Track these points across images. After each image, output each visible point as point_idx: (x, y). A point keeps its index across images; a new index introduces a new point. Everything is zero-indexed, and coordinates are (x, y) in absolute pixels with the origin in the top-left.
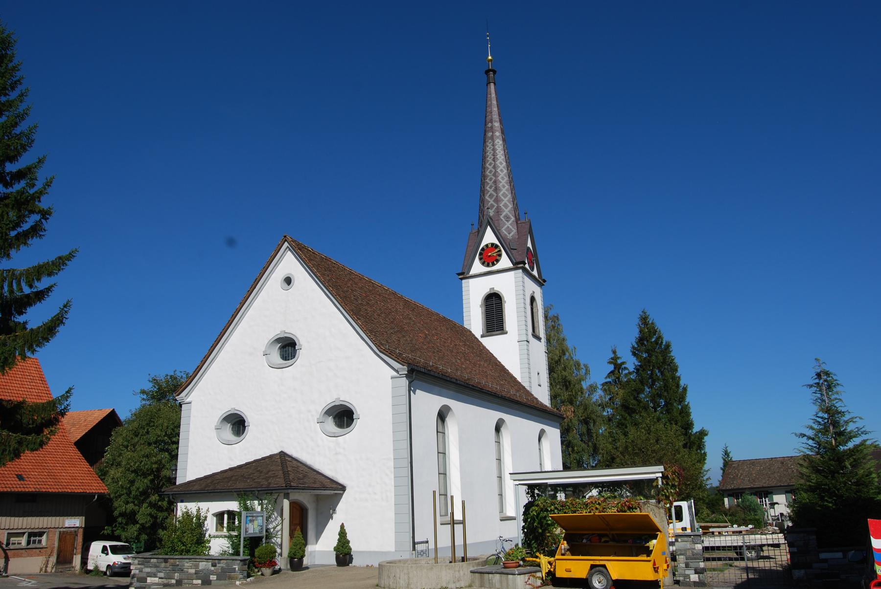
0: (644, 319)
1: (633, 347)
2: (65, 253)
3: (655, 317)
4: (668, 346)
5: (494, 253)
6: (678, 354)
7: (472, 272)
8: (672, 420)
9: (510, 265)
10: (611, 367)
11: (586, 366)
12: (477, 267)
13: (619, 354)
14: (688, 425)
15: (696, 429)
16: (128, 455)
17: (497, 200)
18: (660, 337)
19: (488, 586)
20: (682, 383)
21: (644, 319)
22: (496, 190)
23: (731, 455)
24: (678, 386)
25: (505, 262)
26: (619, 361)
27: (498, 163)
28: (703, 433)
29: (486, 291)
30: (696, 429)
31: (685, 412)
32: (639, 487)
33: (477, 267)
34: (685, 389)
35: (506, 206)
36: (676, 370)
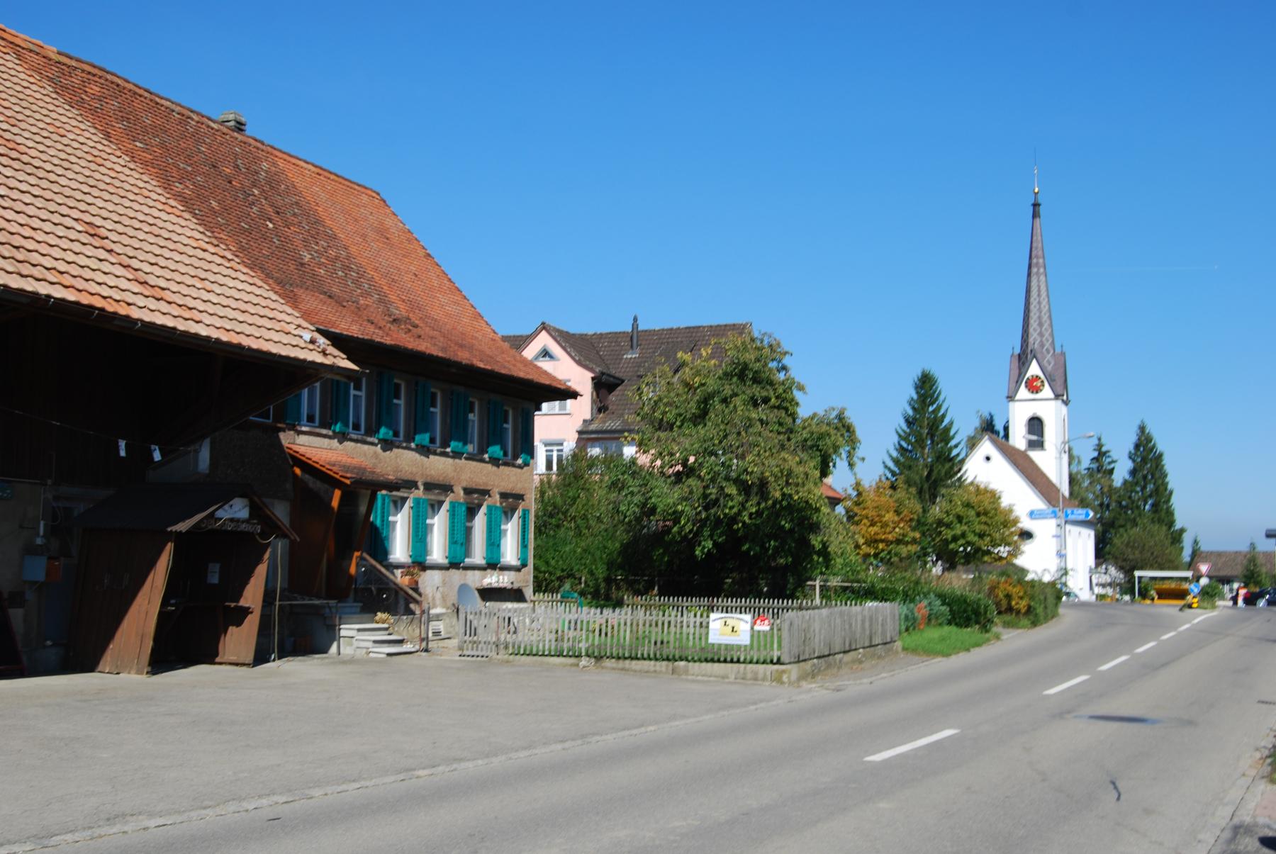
0: (1142, 429)
1: (1130, 452)
2: (388, 203)
3: (1152, 429)
4: (1161, 455)
5: (1038, 384)
6: (1169, 464)
7: (1018, 397)
8: (1160, 521)
9: (1052, 396)
10: (1095, 454)
11: (1078, 457)
12: (1023, 392)
13: (1103, 441)
14: (1171, 523)
15: (1178, 526)
16: (955, 539)
17: (1041, 334)
18: (1154, 446)
19: (757, 628)
20: (1169, 487)
21: (1142, 429)
22: (1041, 325)
23: (1200, 544)
24: (1166, 489)
25: (1047, 392)
26: (1104, 449)
27: (1042, 306)
28: (1182, 531)
29: (1030, 415)
30: (1178, 526)
31: (1170, 513)
32: (1185, 579)
33: (1023, 392)
34: (1171, 493)
35: (1035, 330)
36: (1166, 476)
